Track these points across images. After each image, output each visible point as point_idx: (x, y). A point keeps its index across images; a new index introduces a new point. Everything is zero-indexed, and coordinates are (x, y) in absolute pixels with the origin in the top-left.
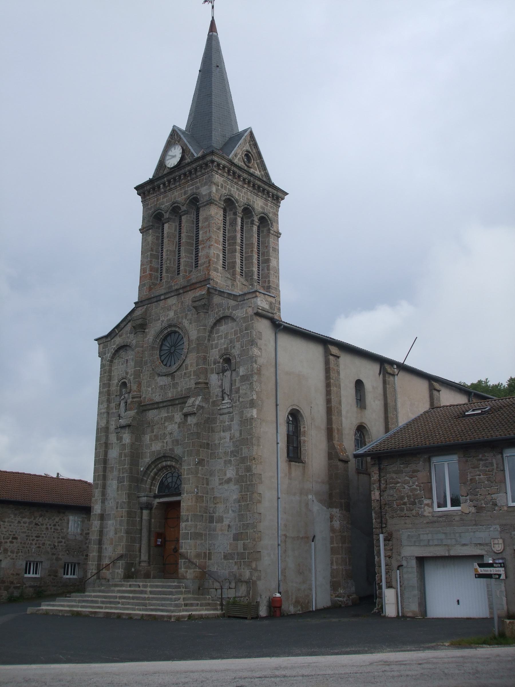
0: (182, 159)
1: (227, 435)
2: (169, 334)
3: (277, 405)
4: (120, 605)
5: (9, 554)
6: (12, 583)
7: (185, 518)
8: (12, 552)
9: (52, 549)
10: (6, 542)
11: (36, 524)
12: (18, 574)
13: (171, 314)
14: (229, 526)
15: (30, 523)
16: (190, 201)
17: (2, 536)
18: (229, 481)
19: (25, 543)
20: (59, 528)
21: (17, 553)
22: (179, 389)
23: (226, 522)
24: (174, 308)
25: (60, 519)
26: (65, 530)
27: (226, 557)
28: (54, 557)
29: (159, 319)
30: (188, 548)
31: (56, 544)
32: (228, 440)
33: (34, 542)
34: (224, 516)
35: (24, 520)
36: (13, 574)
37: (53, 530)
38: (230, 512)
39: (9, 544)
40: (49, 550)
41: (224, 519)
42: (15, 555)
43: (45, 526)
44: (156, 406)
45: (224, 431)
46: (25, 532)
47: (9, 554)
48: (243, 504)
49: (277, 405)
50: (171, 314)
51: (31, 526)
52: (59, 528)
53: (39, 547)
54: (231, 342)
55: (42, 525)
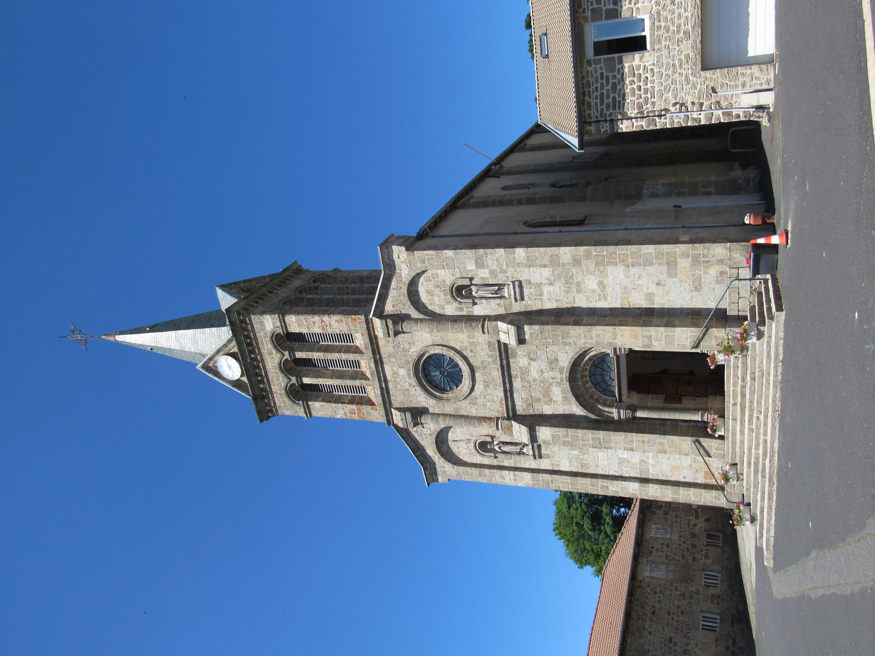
0: (233, 355)
1: (546, 289)
2: (427, 376)
3: (515, 233)
4: (762, 417)
5: (689, 648)
6: (727, 648)
7: (647, 341)
8: (688, 644)
9: (684, 598)
10: (675, 651)
11: (653, 613)
12: (717, 640)
13: (402, 372)
14: (658, 284)
15: (652, 621)
16: (279, 345)
17: (667, 654)
18: (601, 284)
19: (677, 629)
20: (659, 588)
21: (689, 638)
22: (490, 360)
23: (653, 288)
24: (395, 369)
25: (649, 586)
26: (661, 581)
27: (698, 289)
28: (695, 596)
29: (408, 390)
30: (685, 336)
31: (679, 593)
32: (551, 288)
33: (676, 618)
34: (645, 291)
35: (647, 627)
36: (717, 646)
37: (661, 595)
38: (640, 282)
39: (677, 648)
40: (685, 602)
41: (650, 291)
42: (692, 642)
43: (656, 604)
44: (509, 393)
45: (541, 295)
46: (663, 628)
47: (689, 648)
48: (630, 260)
49: (515, 233)
50: (402, 372)
51: (655, 620)
52: (659, 588)
53: (682, 612)
54: (438, 286)
55: (654, 607)
